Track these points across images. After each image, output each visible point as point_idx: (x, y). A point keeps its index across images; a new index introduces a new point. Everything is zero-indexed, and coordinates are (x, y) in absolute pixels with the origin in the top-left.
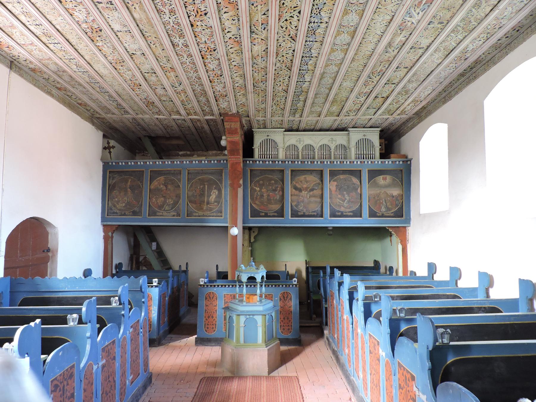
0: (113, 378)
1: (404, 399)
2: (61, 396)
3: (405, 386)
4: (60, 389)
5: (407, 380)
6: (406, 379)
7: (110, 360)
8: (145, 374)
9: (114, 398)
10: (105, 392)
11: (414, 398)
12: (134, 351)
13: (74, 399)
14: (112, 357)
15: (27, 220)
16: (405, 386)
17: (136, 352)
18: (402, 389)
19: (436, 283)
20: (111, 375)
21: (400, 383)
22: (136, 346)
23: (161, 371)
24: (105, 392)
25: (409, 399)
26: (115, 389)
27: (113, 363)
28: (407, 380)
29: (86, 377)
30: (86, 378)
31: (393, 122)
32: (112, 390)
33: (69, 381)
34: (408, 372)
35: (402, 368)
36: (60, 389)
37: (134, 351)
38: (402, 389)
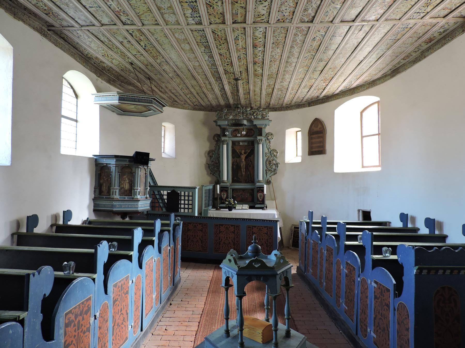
0: (126, 311)
1: (379, 306)
2: (75, 331)
3: (350, 275)
4: (75, 324)
5: (383, 292)
6: (351, 271)
7: (123, 295)
8: (156, 307)
9: (126, 329)
10: (147, 294)
11: (389, 304)
12: (149, 286)
13: (90, 332)
14: (125, 291)
15: (425, 220)
16: (350, 275)
17: (150, 286)
18: (348, 277)
19: (160, 193)
20: (124, 309)
21: (376, 294)
22: (150, 281)
23: (195, 265)
24: (147, 294)
25: (384, 306)
26: (128, 321)
27: (126, 297)
28: (383, 292)
29: (136, 284)
30: (136, 285)
31: (432, 36)
32: (125, 321)
33: (85, 316)
34: (352, 266)
35: (349, 265)
36: (75, 324)
37: (149, 286)
38: (348, 277)
